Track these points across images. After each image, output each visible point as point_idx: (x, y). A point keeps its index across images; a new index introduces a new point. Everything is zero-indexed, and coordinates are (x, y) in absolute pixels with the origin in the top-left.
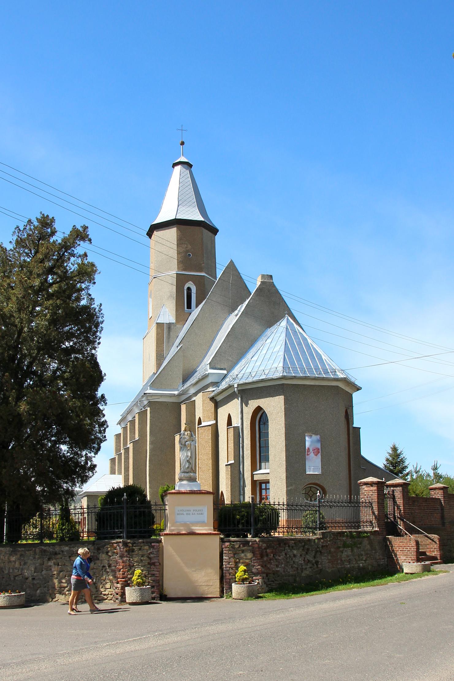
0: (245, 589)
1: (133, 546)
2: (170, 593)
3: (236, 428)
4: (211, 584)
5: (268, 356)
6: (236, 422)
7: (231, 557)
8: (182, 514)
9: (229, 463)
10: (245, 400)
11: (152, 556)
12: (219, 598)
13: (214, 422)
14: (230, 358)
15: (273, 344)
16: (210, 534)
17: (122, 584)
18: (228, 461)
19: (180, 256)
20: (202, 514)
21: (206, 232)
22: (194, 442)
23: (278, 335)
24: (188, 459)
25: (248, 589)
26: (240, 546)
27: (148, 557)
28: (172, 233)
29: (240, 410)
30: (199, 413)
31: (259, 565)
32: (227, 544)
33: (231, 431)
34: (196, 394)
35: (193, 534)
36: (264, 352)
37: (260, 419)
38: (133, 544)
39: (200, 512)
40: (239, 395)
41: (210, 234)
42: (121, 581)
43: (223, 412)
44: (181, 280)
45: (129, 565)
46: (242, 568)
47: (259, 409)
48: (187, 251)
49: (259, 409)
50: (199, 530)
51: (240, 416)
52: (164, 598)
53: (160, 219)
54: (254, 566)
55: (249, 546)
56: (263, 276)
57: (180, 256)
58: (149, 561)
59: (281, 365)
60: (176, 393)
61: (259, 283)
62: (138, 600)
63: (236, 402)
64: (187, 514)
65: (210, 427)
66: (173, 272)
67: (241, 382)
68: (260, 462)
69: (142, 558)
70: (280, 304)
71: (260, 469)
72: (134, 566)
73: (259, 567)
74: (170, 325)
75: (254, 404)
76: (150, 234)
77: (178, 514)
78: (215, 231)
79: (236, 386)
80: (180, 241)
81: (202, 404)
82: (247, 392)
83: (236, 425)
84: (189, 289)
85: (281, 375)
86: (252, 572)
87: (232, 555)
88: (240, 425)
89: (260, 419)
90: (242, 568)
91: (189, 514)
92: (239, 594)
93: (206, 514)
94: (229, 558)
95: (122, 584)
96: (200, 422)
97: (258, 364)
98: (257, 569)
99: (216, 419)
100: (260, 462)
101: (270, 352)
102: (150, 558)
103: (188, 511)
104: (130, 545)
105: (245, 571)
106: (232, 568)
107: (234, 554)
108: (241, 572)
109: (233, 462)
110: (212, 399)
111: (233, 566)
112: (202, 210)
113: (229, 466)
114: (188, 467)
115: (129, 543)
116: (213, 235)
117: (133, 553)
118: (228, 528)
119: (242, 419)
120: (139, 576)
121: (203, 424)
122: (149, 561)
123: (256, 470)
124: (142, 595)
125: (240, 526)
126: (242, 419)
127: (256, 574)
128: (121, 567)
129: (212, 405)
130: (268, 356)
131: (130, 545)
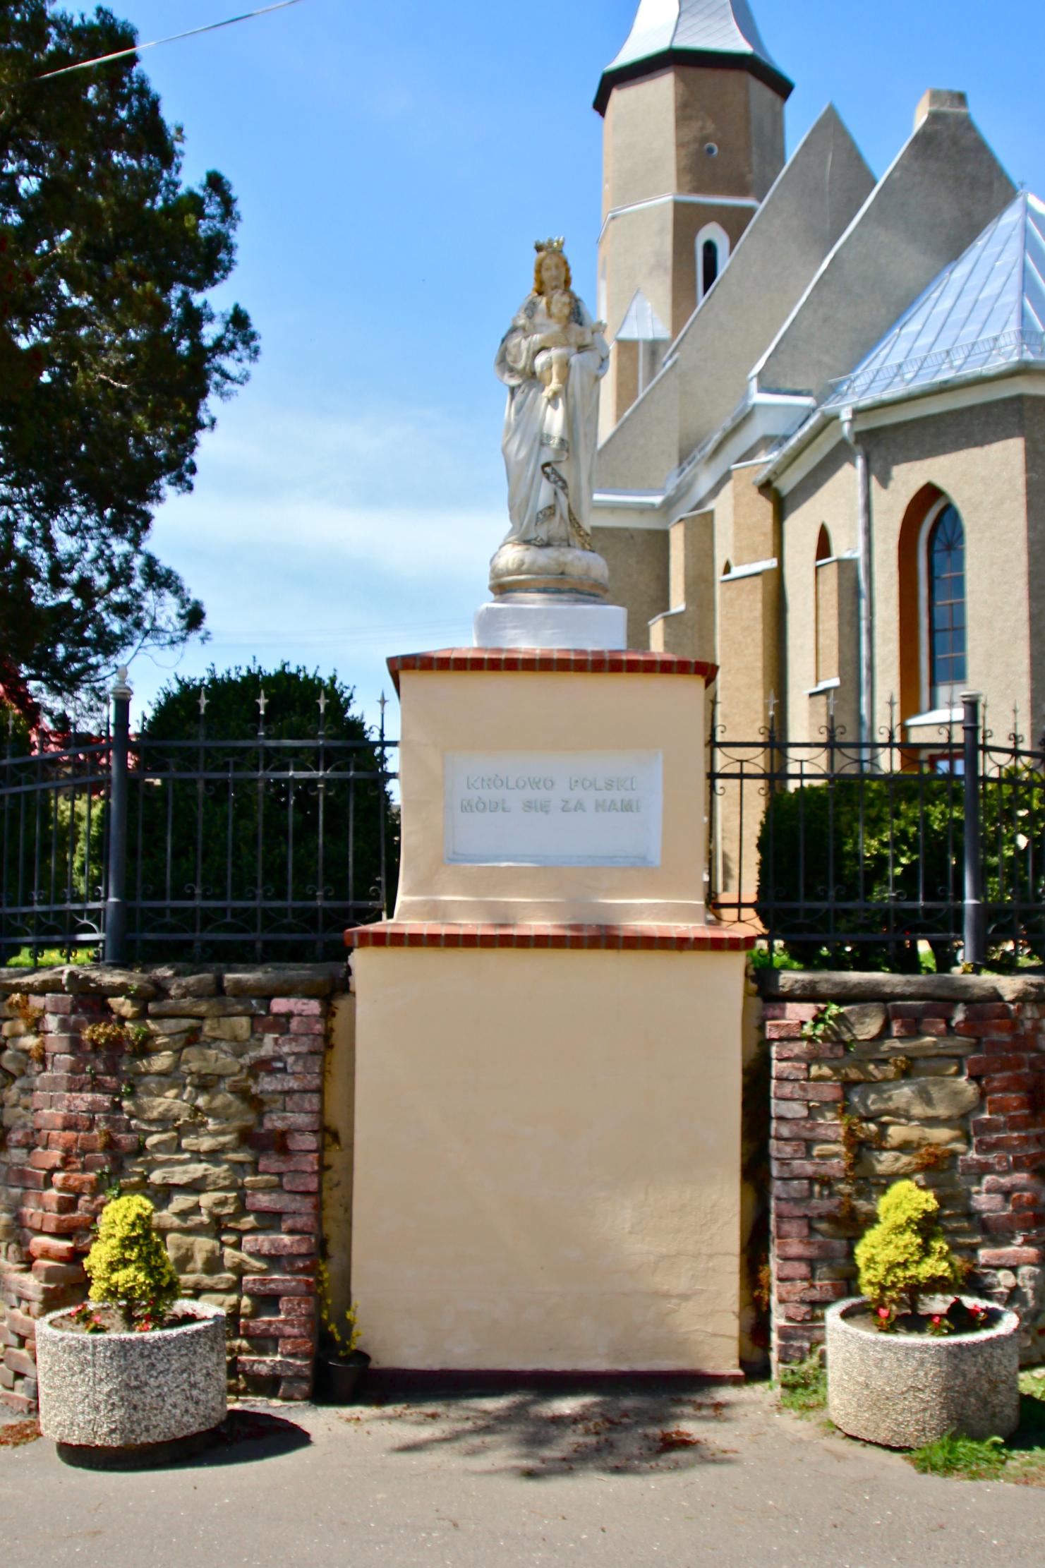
0: (930, 1376)
1: (142, 1015)
2: (393, 1339)
3: (846, 566)
4: (681, 1285)
5: (959, 315)
6: (846, 546)
7: (826, 1105)
8: (499, 806)
9: (821, 686)
10: (877, 465)
11: (267, 1084)
12: (735, 1381)
13: (772, 563)
14: (826, 359)
15: (976, 281)
16: (681, 944)
17: (50, 1275)
18: (817, 681)
19: (683, 152)
20: (627, 807)
21: (758, 90)
22: (589, 358)
23: (993, 249)
24: (547, 456)
25: (956, 1372)
26: (885, 1033)
27: (243, 1094)
28: (662, 91)
29: (860, 501)
30: (723, 550)
31: (1017, 1166)
32: (800, 1012)
33: (830, 576)
34: (715, 491)
35: (606, 939)
36: (946, 304)
37: (932, 529)
38: (141, 998)
39: (618, 795)
40: (858, 449)
41: (769, 94)
42: (46, 1254)
43: (800, 529)
44: (686, 220)
45: (111, 1145)
46: (907, 1199)
47: (929, 494)
48: (703, 140)
49: (929, 494)
50: (647, 913)
51: (860, 523)
52: (344, 1374)
53: (630, 53)
54: (985, 1169)
55: (950, 1030)
56: (935, 96)
57: (683, 152)
58: (250, 1119)
59: (1013, 327)
60: (657, 500)
61: (920, 119)
62: (103, 1435)
63: (851, 475)
64: (529, 806)
65: (758, 581)
66: (662, 200)
67: (866, 401)
68: (933, 684)
69: (201, 1101)
70: (990, 184)
71: (933, 706)
72: (141, 1150)
73: (1021, 1177)
74: (654, 348)
75: (910, 477)
76: (601, 105)
77: (466, 807)
78: (782, 87)
79: (846, 415)
80: (684, 111)
81: (735, 516)
82: (884, 439)
83: (847, 555)
84: (710, 248)
85: (1015, 358)
86: (970, 1214)
87: (830, 1092)
88: (859, 554)
89: (932, 529)
90: (907, 1199)
91: (544, 808)
92: (879, 1402)
93: (654, 805)
94: (812, 1113)
95: (50, 1275)
96: (727, 569)
97: (925, 341)
98: (1007, 1193)
99: (779, 552)
100: (933, 684)
101: (967, 300)
102: (256, 1103)
103: (535, 784)
104: (124, 1006)
105: (927, 1226)
106: (826, 1182)
107: (848, 1085)
108: (899, 1229)
109: (835, 682)
110: (766, 488)
111: (837, 1166)
112: (748, 28)
113: (822, 698)
114: (551, 510)
115: (120, 990)
116: (779, 100)
117: (143, 1065)
118: (804, 904)
119: (868, 531)
120: (127, 1243)
121: (736, 572)
122: (250, 1119)
123: (917, 711)
124: (130, 1391)
125: (885, 895)
126: (868, 531)
127: (996, 1233)
128: (54, 1156)
129: (765, 507)
130: (959, 315)
131: (124, 1006)
